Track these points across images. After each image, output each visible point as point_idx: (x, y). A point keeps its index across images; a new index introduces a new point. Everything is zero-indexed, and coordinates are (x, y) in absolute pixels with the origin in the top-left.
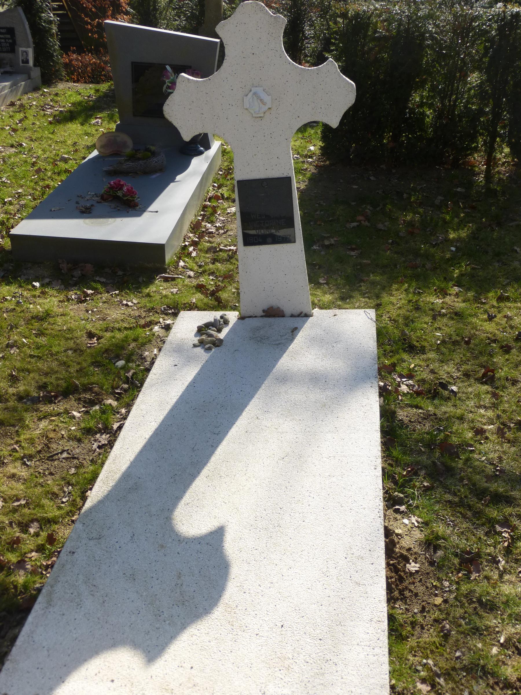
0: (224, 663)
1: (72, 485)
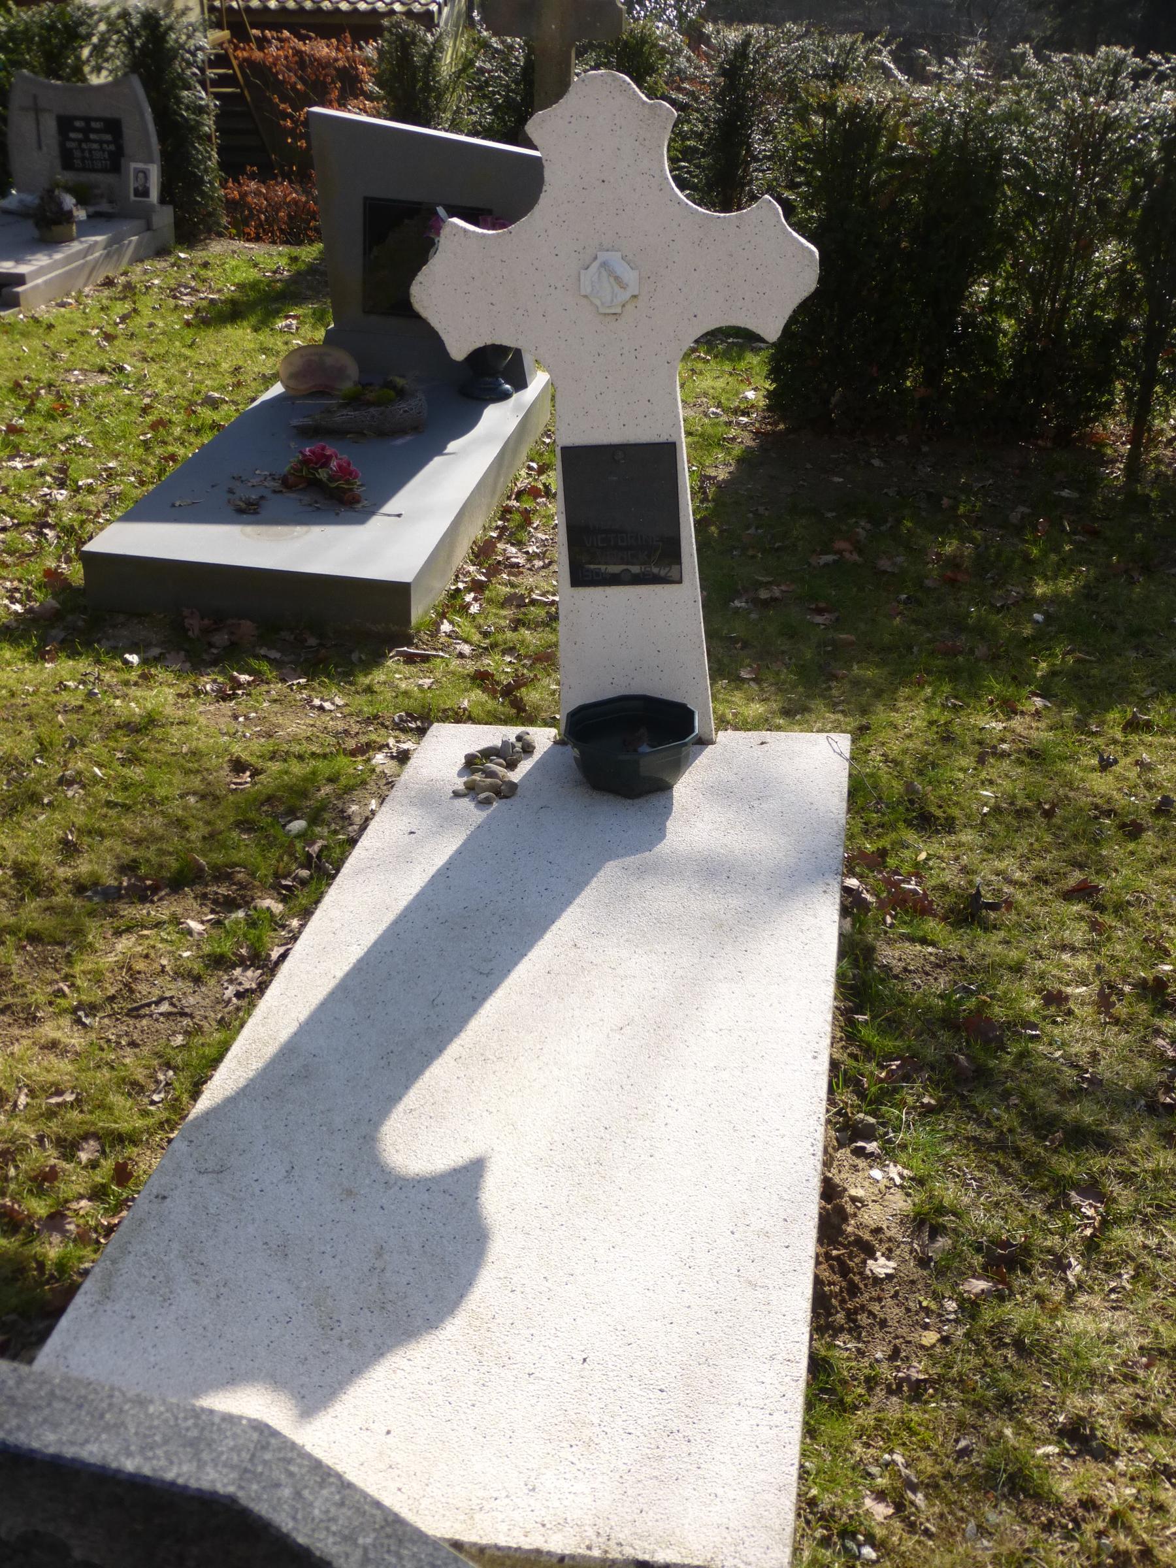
0: (455, 1427)
1: (175, 1069)
